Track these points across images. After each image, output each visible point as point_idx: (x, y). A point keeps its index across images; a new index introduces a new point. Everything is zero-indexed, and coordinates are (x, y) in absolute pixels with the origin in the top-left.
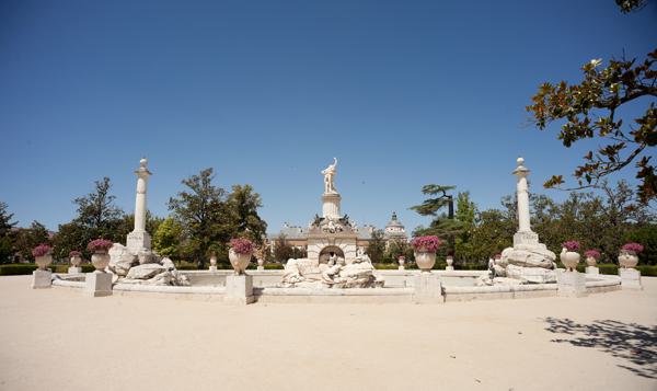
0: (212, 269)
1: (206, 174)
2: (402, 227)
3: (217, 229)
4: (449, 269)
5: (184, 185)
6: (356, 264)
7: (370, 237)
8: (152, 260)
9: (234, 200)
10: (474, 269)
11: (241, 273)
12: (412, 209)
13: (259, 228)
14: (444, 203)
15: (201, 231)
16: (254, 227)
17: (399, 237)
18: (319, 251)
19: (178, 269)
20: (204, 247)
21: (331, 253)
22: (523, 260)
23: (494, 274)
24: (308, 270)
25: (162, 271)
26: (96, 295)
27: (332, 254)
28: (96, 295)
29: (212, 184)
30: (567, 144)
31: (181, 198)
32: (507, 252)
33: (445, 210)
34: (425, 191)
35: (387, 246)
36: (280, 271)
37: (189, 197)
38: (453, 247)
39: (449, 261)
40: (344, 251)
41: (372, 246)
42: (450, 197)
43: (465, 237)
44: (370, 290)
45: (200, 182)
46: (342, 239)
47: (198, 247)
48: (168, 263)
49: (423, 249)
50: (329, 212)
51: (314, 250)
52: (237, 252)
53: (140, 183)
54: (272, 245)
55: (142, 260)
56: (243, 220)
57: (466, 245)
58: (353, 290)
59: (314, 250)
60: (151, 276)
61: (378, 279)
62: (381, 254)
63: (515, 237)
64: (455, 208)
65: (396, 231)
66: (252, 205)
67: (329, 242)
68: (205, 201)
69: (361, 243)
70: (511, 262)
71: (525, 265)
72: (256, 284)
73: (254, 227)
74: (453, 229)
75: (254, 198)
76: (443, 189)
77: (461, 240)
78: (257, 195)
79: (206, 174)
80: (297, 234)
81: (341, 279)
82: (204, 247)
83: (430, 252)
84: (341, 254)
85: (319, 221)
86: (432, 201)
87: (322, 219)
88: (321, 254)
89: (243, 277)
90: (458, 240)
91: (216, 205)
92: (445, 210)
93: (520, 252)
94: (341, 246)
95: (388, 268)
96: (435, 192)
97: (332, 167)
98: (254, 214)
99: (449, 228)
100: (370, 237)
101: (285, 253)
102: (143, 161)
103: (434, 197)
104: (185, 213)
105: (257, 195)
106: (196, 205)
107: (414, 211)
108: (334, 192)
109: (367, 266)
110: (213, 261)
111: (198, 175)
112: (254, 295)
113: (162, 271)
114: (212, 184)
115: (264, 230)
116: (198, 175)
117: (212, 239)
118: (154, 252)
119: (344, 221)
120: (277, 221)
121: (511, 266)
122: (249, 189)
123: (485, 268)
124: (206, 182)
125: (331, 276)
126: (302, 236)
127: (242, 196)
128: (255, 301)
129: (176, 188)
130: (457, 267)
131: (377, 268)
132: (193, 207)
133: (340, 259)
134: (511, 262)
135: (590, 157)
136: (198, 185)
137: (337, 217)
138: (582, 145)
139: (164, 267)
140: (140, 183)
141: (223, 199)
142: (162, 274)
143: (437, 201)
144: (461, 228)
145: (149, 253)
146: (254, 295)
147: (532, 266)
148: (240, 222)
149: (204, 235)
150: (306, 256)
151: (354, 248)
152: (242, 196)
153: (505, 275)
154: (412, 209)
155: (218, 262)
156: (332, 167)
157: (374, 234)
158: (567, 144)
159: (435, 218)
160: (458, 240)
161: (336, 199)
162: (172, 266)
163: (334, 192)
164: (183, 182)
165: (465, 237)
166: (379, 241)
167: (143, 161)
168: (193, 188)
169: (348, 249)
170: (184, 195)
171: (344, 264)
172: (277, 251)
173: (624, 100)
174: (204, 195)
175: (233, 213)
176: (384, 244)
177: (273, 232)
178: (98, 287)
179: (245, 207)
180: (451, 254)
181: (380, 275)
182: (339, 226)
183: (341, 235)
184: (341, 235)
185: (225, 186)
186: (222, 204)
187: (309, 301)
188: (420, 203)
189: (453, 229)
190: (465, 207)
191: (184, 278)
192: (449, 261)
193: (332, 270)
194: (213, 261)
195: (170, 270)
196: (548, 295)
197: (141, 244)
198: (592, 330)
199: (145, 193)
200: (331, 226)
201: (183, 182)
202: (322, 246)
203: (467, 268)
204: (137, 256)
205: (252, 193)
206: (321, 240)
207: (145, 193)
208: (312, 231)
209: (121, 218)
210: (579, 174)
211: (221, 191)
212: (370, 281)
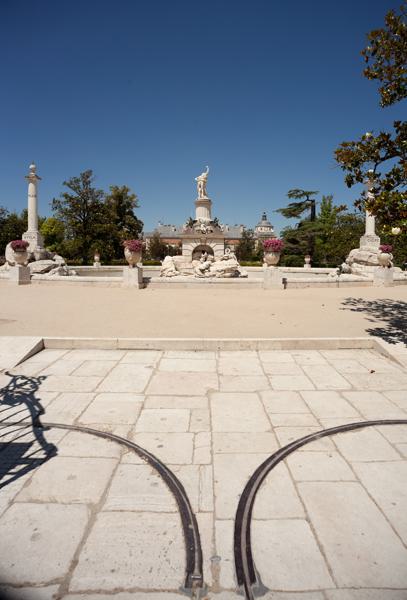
0: (96, 265)
1: (86, 176)
2: (272, 227)
3: (99, 228)
4: (307, 267)
5: (66, 186)
6: (224, 260)
7: (240, 236)
8: (46, 257)
9: (112, 201)
10: (330, 267)
11: (134, 266)
12: (277, 211)
13: (136, 227)
14: (307, 207)
15: (84, 230)
16: (131, 226)
17: (268, 236)
18: (192, 249)
19: (69, 264)
20: (86, 246)
21: (202, 251)
22: (365, 259)
23: (341, 271)
24: (183, 266)
25: (56, 266)
26: (20, 283)
27: (203, 252)
28: (20, 283)
29: (92, 186)
30: (349, 186)
31: (63, 199)
32: (354, 253)
33: (306, 214)
34: (290, 196)
35: (256, 245)
36: (157, 267)
37: (71, 199)
38: (312, 248)
39: (307, 260)
40: (214, 249)
41: (242, 245)
42: (313, 201)
43: (325, 239)
44: (235, 279)
45: (81, 184)
46: (212, 240)
47: (81, 244)
48: (59, 260)
49: (270, 249)
50: (202, 215)
51: (188, 248)
52: (131, 250)
53: (31, 187)
54: (147, 243)
55: (37, 256)
56: (121, 220)
57: (326, 246)
58: (214, 279)
59: (188, 248)
60: (47, 271)
61: (242, 274)
62: (248, 252)
63: (362, 239)
64: (318, 211)
65: (265, 230)
66: (129, 205)
67: (201, 241)
68: (85, 202)
69: (231, 242)
70: (356, 261)
71: (367, 263)
72: (145, 275)
73: (131, 226)
74: (314, 231)
75: (131, 199)
76: (307, 194)
77: (321, 241)
78: (134, 196)
79: (86, 176)
80: (171, 232)
81: (211, 273)
82: (86, 246)
83: (275, 251)
84: (211, 252)
85: (192, 223)
86: (296, 205)
87: (195, 222)
88: (194, 252)
89: (136, 270)
90: (319, 241)
91: (96, 207)
92: (306, 214)
93: (363, 253)
94: (212, 245)
95: (254, 265)
96: (299, 196)
97: (204, 175)
98: (131, 213)
99: (309, 229)
100: (240, 236)
101: (159, 251)
102: (32, 166)
103: (298, 201)
104: (65, 212)
105: (134, 196)
106: (78, 206)
107: (280, 214)
108: (206, 198)
109: (233, 262)
110: (96, 258)
111: (79, 177)
112: (144, 282)
113: (56, 266)
114: (92, 186)
115: (140, 230)
116: (79, 177)
117: (94, 238)
118: (47, 250)
119: (214, 223)
120: (153, 220)
121: (355, 264)
122: (126, 190)
123: (335, 267)
124: (87, 183)
125: (202, 271)
126: (176, 234)
127: (120, 197)
128: (144, 287)
129: (59, 190)
130: (313, 264)
131: (242, 265)
132: (75, 208)
133: (210, 256)
134: (356, 261)
135: (364, 194)
136: (79, 187)
137: (208, 220)
138: (357, 187)
139: (56, 263)
140: (31, 187)
141: (102, 200)
142: (57, 269)
143: (300, 204)
144: (321, 230)
145: (43, 250)
146: (144, 282)
147: (373, 265)
148: (117, 221)
149: (85, 234)
150: (180, 253)
151: (222, 247)
152: (120, 197)
153: (349, 272)
154: (277, 211)
155: (101, 259)
156: (204, 175)
157: (244, 234)
158: (349, 186)
159: (299, 221)
160: (319, 241)
161: (207, 204)
162: (63, 262)
163: (206, 198)
164: (65, 183)
165: (325, 239)
166: (248, 239)
167: (32, 166)
168: (75, 189)
169: (218, 247)
170: (66, 196)
171: (213, 261)
172: (152, 249)
173: (383, 159)
174: (85, 197)
175: (112, 214)
176: (254, 243)
177: (148, 230)
178: (20, 278)
179: (123, 205)
180: (311, 254)
181: (243, 270)
182: (209, 228)
183: (211, 235)
184: (211, 235)
185: (104, 187)
186: (102, 205)
187: (186, 287)
188: (285, 206)
189: (314, 231)
190: (326, 209)
191: (74, 272)
192: (307, 260)
193: (203, 266)
194: (96, 258)
195: (62, 265)
196: (365, 286)
197: (36, 243)
198: (371, 304)
199: (36, 196)
200: (202, 228)
201: (65, 183)
202: (195, 245)
203: (324, 266)
204: (32, 254)
205: (129, 194)
206: (194, 240)
207: (36, 196)
208: (187, 232)
209: (6, 217)
210: (356, 204)
211: (101, 193)
212: (236, 274)
